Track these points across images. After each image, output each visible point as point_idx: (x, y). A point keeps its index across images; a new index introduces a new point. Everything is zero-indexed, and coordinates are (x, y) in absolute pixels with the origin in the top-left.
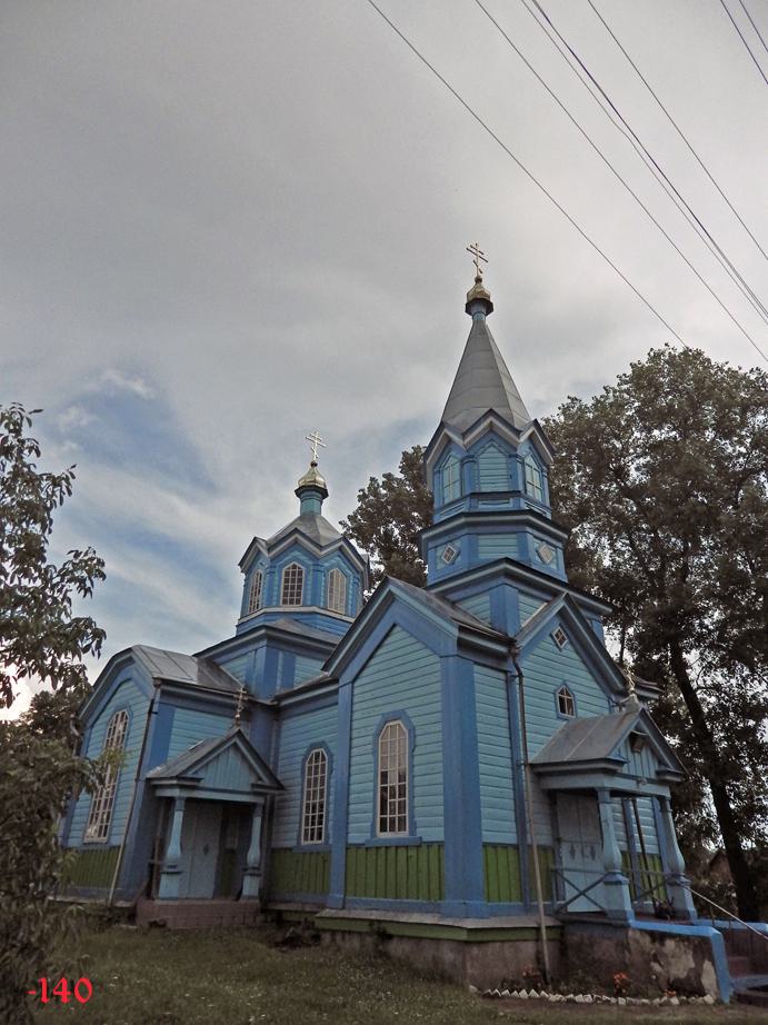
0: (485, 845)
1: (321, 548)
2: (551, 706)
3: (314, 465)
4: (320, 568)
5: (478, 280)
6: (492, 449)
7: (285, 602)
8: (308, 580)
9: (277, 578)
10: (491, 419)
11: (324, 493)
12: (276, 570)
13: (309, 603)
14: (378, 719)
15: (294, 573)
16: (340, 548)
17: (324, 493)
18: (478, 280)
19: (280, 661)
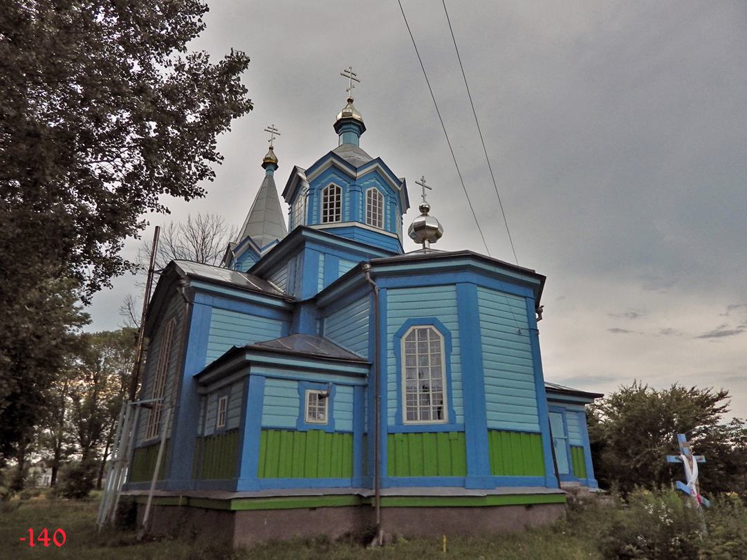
0: (490, 430)
1: (356, 170)
2: (120, 444)
3: (350, 101)
4: (357, 188)
5: (271, 148)
6: (249, 258)
7: (325, 220)
8: (345, 198)
9: (315, 199)
10: (249, 242)
11: (361, 128)
12: (315, 191)
13: (347, 219)
14: (403, 320)
15: (332, 192)
16: (376, 171)
17: (361, 128)
18: (271, 148)
19: (321, 264)
